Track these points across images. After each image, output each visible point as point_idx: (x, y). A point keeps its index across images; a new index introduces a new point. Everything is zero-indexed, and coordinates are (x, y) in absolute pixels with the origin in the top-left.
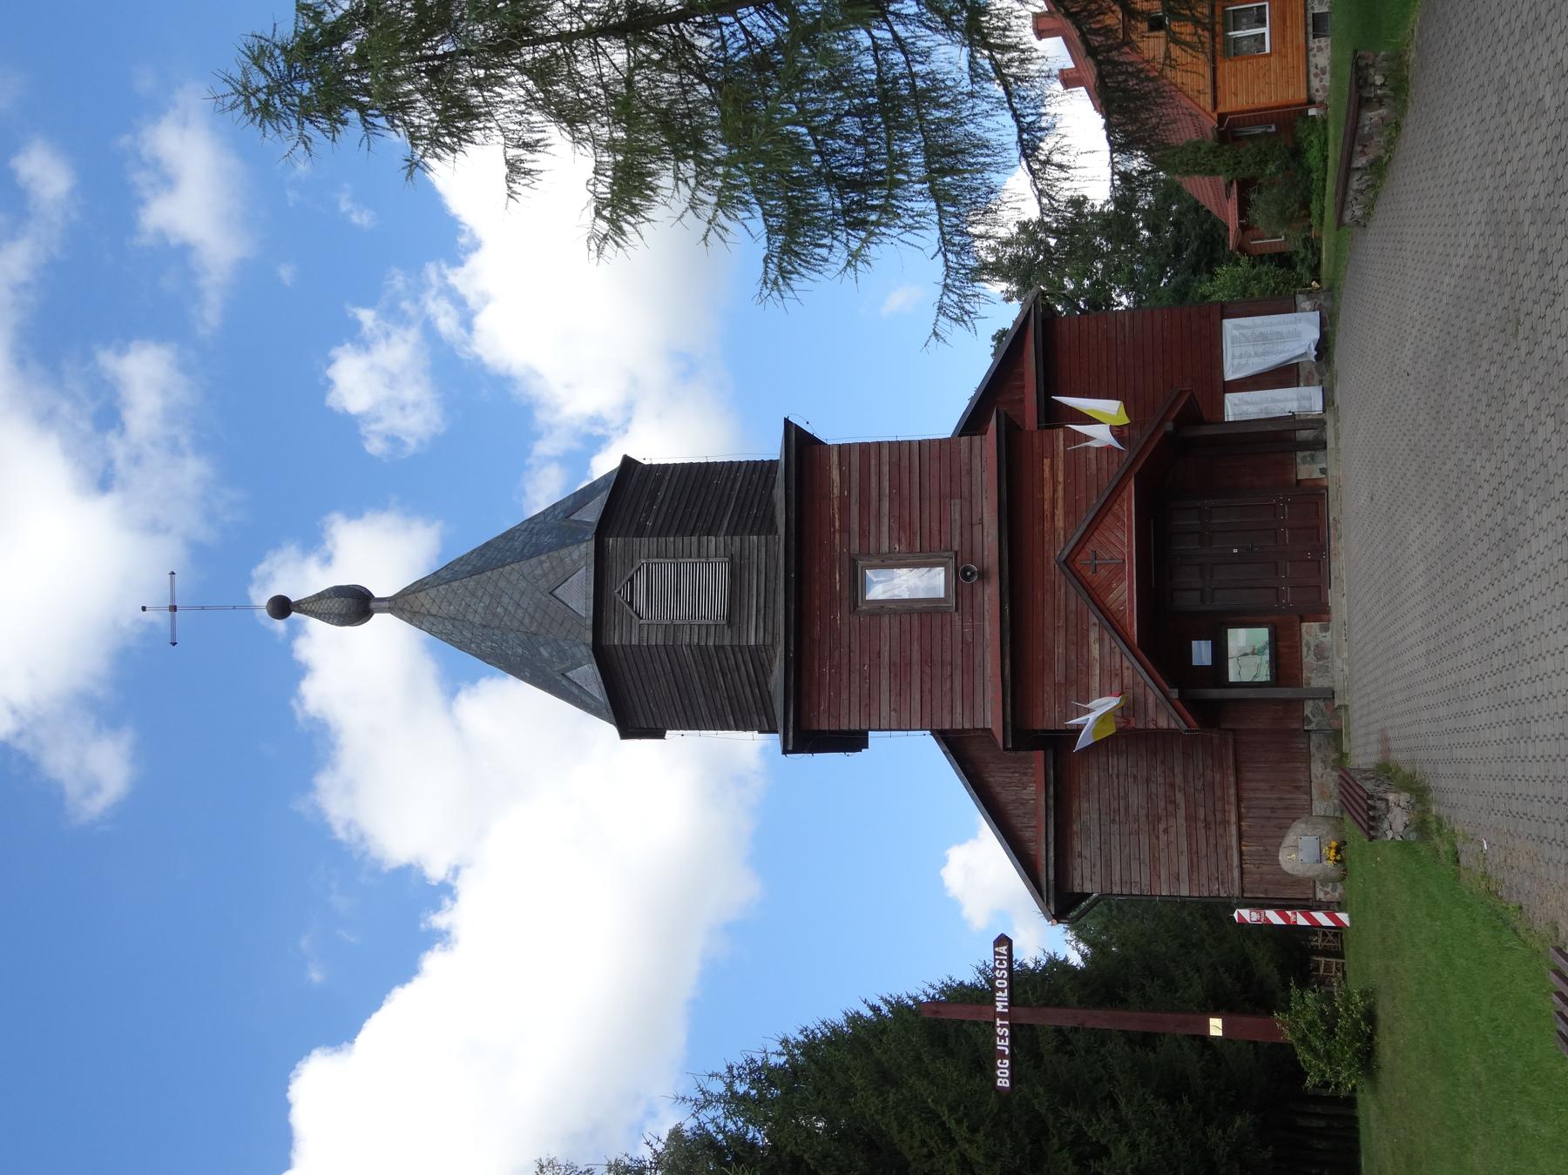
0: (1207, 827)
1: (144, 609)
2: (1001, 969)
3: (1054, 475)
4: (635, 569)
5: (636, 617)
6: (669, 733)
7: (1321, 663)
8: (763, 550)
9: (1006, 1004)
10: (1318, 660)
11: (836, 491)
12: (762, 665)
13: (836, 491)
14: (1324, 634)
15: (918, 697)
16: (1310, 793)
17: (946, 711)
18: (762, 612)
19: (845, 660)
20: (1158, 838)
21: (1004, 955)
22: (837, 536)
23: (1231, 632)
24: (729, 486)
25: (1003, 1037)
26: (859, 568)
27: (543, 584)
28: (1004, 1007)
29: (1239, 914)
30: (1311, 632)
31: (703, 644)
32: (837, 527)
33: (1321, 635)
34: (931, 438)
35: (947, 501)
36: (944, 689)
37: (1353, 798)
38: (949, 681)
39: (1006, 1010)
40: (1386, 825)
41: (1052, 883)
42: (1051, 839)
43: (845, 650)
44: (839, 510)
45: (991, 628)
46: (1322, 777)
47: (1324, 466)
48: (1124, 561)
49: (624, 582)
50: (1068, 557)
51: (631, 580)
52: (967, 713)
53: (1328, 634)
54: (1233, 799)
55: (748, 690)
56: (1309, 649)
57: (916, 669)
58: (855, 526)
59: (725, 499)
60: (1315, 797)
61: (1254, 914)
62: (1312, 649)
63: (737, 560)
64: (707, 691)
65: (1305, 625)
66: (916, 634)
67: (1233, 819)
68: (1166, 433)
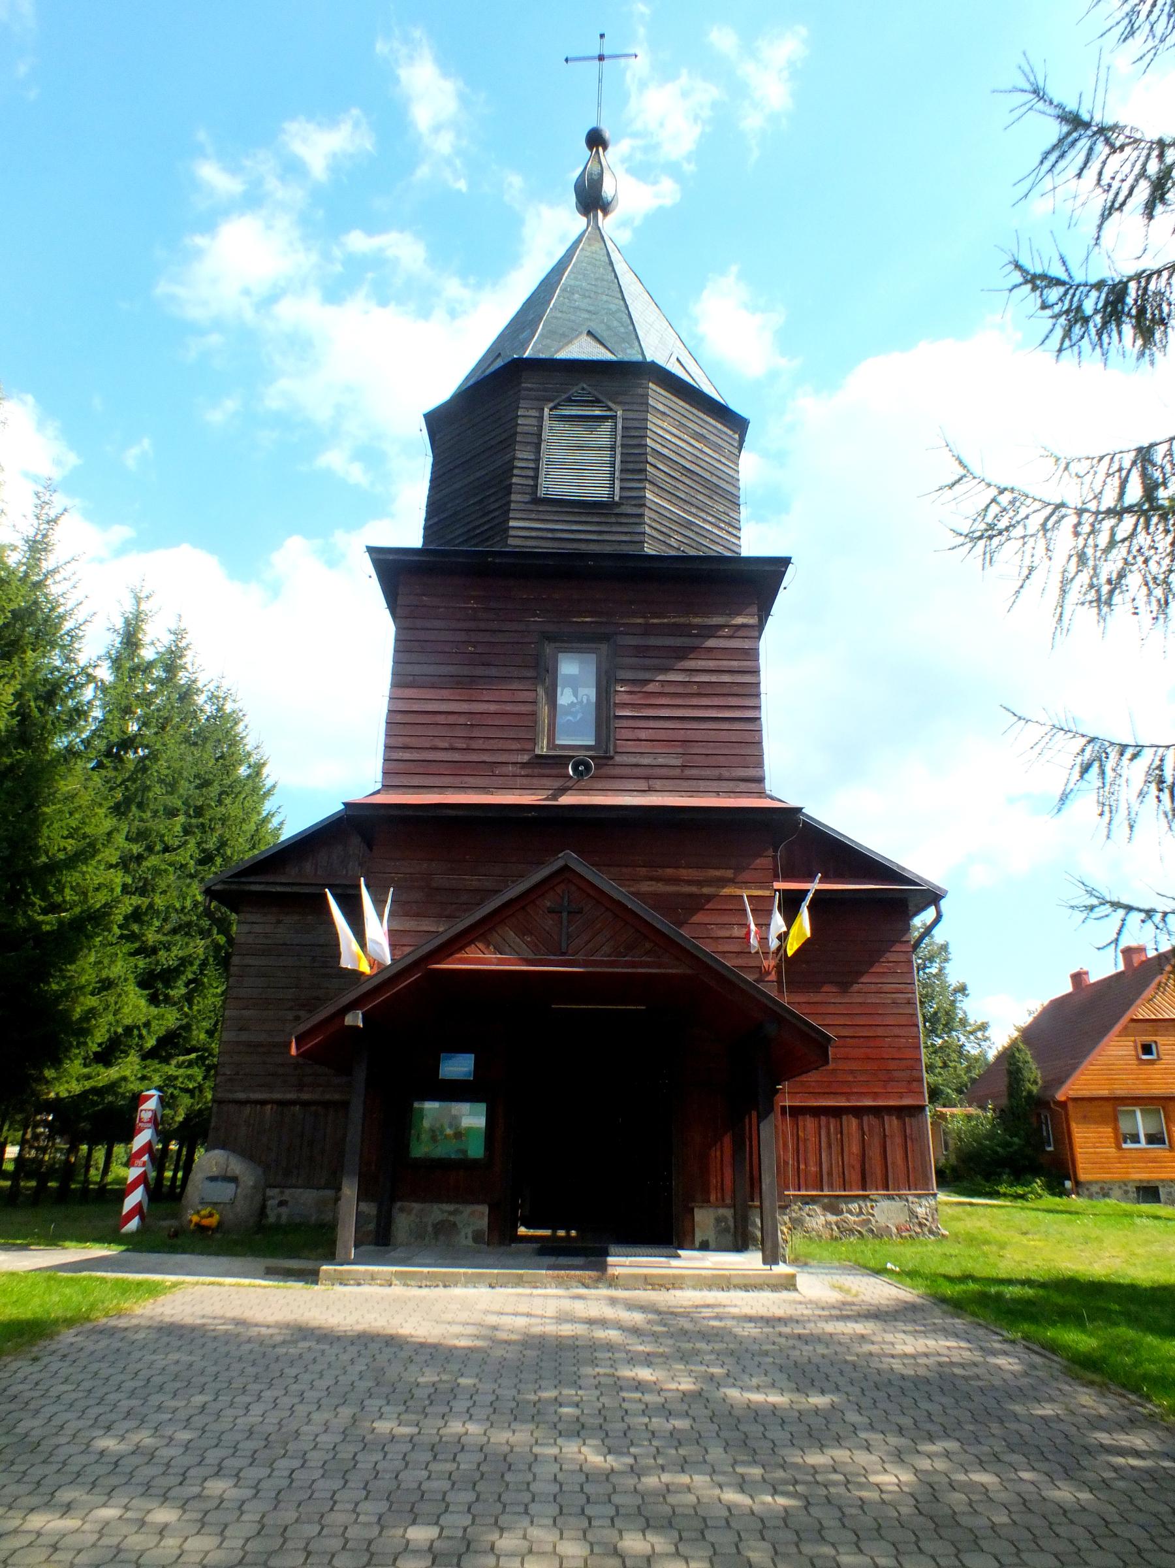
1: (602, 36)
7: (430, 1229)
10: (435, 1226)
11: (697, 620)
13: (697, 620)
14: (470, 1235)
16: (325, 1187)
18: (550, 535)
19: (482, 625)
20: (291, 1009)
22: (640, 621)
23: (482, 1107)
24: (710, 519)
30: (477, 1217)
31: (516, 472)
33: (469, 1231)
34: (764, 744)
36: (436, 739)
38: (446, 745)
41: (247, 888)
42: (295, 889)
43: (495, 625)
44: (674, 624)
48: (564, 954)
49: (596, 393)
50: (573, 871)
51: (598, 401)
52: (401, 765)
53: (470, 1242)
54: (328, 1097)
56: (451, 1213)
58: (653, 641)
60: (322, 1193)
61: (149, 1114)
62: (451, 1218)
65: (484, 1209)
66: (509, 708)
67: (305, 1096)
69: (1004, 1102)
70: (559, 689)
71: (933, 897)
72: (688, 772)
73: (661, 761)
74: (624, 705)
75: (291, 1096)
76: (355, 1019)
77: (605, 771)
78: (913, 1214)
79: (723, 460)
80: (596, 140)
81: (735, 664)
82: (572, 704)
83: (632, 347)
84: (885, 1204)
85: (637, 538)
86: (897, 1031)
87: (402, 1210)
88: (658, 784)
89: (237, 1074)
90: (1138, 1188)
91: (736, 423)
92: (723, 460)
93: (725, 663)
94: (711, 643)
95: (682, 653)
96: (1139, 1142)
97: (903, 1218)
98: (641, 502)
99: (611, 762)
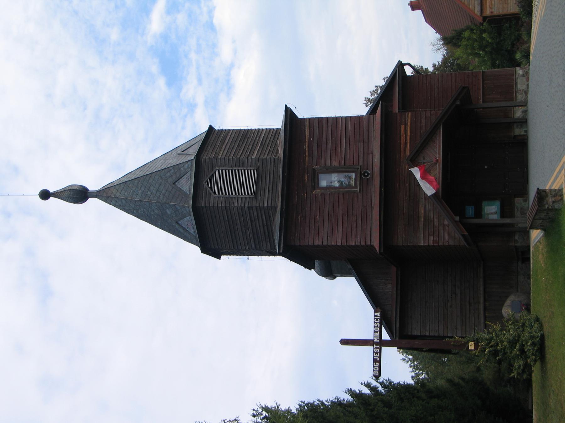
2: (377, 323)
4: (213, 172)
5: (213, 194)
8: (273, 164)
9: (379, 338)
11: (307, 138)
12: (270, 216)
13: (307, 138)
14: (524, 203)
15: (341, 230)
17: (353, 237)
18: (271, 192)
21: (378, 316)
22: (307, 158)
26: (316, 173)
27: (170, 180)
28: (378, 339)
31: (243, 205)
32: (307, 154)
33: (523, 204)
37: (535, 207)
39: (378, 341)
40: (545, 202)
41: (398, 329)
42: (398, 310)
44: (308, 147)
45: (376, 200)
46: (523, 282)
47: (525, 129)
49: (208, 178)
51: (211, 177)
55: (262, 230)
56: (518, 210)
58: (315, 153)
59: (256, 143)
63: (260, 169)
65: (516, 199)
69: (518, 201)
71: (400, 66)
74: (340, 162)
75: (481, 306)
78: (523, 76)
80: (45, 195)
81: (325, 126)
84: (516, 11)
85: (273, 160)
91: (211, 128)
93: (324, 128)
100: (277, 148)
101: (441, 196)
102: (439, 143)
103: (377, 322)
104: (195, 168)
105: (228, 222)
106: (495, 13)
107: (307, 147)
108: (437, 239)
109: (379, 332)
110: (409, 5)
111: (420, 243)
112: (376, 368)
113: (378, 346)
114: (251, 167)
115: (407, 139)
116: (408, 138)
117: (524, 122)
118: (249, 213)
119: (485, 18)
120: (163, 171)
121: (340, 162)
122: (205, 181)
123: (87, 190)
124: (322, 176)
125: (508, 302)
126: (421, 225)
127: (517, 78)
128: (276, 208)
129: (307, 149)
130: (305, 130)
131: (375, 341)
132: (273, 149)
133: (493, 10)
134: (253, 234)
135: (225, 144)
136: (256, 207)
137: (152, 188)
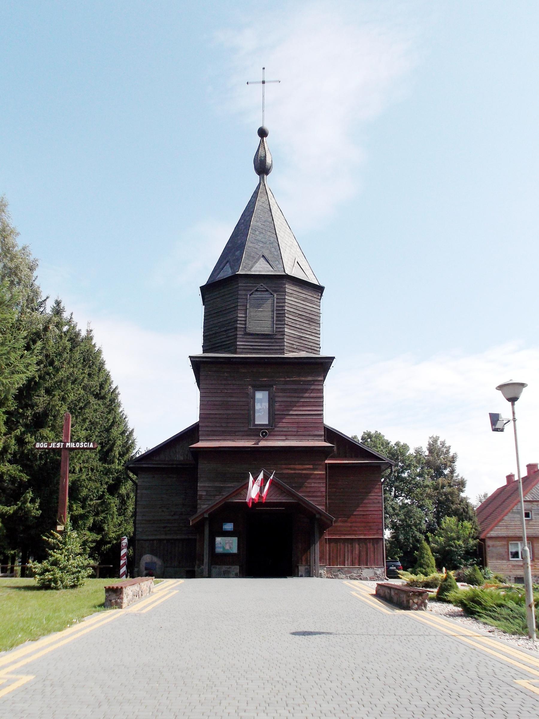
0: (165, 527)
1: (264, 68)
3: (305, 469)
5: (251, 293)
6: (204, 306)
7: (222, 572)
9: (69, 447)
10: (224, 572)
11: (303, 379)
12: (229, 347)
13: (303, 379)
14: (234, 574)
17: (207, 424)
18: (251, 347)
21: (89, 446)
22: (283, 379)
25: (56, 445)
29: (125, 538)
30: (236, 569)
31: (238, 322)
33: (234, 573)
35: (296, 426)
39: (67, 447)
42: (159, 466)
49: (266, 288)
51: (267, 291)
55: (219, 341)
57: (226, 412)
59: (302, 331)
61: (125, 544)
62: (229, 570)
64: (219, 324)
65: (238, 567)
68: (315, 515)
70: (256, 403)
72: (299, 433)
73: (290, 429)
74: (278, 410)
75: (163, 537)
76: (206, 516)
77: (272, 433)
78: (376, 574)
79: (314, 306)
80: (262, 133)
82: (260, 409)
83: (279, 263)
84: (366, 570)
85: (282, 348)
86: (374, 512)
87: (214, 568)
88: (289, 437)
89: (143, 531)
90: (515, 578)
92: (314, 306)
94: (313, 387)
95: (306, 391)
96: (518, 557)
97: (372, 575)
98: (283, 333)
99: (274, 430)
100: (296, 351)
101: (229, 501)
102: (280, 499)
103: (85, 445)
104: (277, 275)
105: (225, 310)
106: (488, 549)
107: (294, 379)
108: (203, 499)
109: (75, 447)
110: (511, 473)
111: (200, 483)
112: (43, 445)
113: (62, 447)
114: (276, 327)
115: (299, 470)
116: (300, 472)
117: (309, 574)
118: (232, 329)
119: (483, 540)
120: (277, 245)
121: (278, 410)
122: (262, 284)
123: (267, 174)
124: (266, 393)
125: (155, 559)
126: (217, 484)
127: (374, 569)
128: (235, 353)
129: (292, 379)
130: (311, 376)
131: (67, 444)
132: (296, 347)
133: (491, 548)
134: (216, 333)
135: (302, 302)
136: (237, 334)
137: (262, 235)
